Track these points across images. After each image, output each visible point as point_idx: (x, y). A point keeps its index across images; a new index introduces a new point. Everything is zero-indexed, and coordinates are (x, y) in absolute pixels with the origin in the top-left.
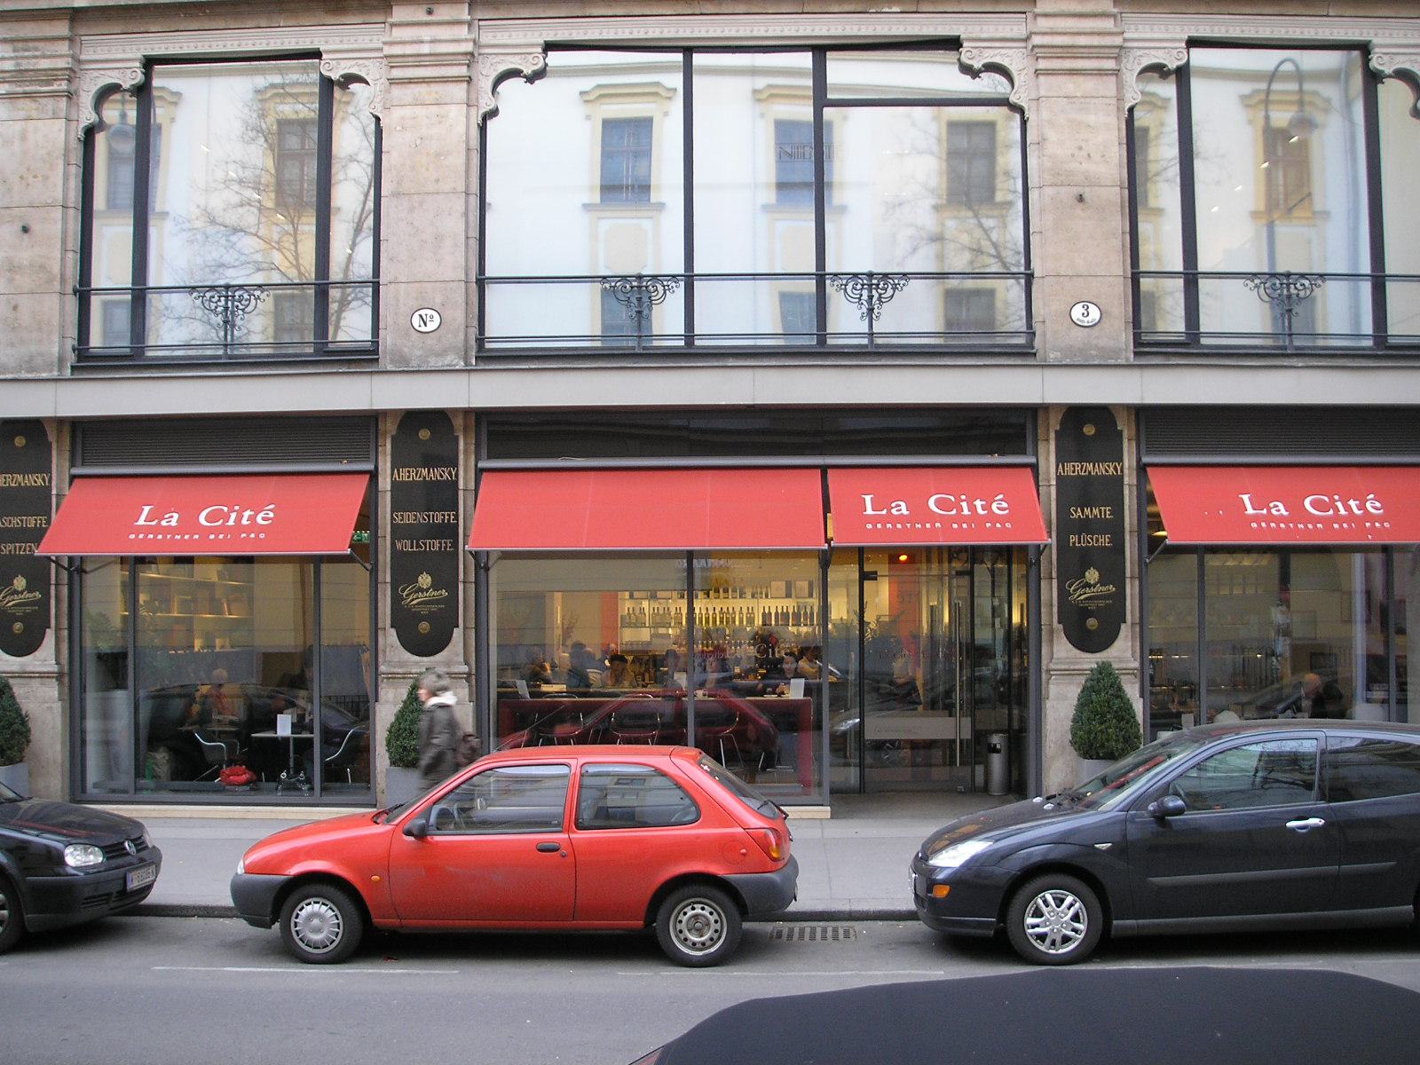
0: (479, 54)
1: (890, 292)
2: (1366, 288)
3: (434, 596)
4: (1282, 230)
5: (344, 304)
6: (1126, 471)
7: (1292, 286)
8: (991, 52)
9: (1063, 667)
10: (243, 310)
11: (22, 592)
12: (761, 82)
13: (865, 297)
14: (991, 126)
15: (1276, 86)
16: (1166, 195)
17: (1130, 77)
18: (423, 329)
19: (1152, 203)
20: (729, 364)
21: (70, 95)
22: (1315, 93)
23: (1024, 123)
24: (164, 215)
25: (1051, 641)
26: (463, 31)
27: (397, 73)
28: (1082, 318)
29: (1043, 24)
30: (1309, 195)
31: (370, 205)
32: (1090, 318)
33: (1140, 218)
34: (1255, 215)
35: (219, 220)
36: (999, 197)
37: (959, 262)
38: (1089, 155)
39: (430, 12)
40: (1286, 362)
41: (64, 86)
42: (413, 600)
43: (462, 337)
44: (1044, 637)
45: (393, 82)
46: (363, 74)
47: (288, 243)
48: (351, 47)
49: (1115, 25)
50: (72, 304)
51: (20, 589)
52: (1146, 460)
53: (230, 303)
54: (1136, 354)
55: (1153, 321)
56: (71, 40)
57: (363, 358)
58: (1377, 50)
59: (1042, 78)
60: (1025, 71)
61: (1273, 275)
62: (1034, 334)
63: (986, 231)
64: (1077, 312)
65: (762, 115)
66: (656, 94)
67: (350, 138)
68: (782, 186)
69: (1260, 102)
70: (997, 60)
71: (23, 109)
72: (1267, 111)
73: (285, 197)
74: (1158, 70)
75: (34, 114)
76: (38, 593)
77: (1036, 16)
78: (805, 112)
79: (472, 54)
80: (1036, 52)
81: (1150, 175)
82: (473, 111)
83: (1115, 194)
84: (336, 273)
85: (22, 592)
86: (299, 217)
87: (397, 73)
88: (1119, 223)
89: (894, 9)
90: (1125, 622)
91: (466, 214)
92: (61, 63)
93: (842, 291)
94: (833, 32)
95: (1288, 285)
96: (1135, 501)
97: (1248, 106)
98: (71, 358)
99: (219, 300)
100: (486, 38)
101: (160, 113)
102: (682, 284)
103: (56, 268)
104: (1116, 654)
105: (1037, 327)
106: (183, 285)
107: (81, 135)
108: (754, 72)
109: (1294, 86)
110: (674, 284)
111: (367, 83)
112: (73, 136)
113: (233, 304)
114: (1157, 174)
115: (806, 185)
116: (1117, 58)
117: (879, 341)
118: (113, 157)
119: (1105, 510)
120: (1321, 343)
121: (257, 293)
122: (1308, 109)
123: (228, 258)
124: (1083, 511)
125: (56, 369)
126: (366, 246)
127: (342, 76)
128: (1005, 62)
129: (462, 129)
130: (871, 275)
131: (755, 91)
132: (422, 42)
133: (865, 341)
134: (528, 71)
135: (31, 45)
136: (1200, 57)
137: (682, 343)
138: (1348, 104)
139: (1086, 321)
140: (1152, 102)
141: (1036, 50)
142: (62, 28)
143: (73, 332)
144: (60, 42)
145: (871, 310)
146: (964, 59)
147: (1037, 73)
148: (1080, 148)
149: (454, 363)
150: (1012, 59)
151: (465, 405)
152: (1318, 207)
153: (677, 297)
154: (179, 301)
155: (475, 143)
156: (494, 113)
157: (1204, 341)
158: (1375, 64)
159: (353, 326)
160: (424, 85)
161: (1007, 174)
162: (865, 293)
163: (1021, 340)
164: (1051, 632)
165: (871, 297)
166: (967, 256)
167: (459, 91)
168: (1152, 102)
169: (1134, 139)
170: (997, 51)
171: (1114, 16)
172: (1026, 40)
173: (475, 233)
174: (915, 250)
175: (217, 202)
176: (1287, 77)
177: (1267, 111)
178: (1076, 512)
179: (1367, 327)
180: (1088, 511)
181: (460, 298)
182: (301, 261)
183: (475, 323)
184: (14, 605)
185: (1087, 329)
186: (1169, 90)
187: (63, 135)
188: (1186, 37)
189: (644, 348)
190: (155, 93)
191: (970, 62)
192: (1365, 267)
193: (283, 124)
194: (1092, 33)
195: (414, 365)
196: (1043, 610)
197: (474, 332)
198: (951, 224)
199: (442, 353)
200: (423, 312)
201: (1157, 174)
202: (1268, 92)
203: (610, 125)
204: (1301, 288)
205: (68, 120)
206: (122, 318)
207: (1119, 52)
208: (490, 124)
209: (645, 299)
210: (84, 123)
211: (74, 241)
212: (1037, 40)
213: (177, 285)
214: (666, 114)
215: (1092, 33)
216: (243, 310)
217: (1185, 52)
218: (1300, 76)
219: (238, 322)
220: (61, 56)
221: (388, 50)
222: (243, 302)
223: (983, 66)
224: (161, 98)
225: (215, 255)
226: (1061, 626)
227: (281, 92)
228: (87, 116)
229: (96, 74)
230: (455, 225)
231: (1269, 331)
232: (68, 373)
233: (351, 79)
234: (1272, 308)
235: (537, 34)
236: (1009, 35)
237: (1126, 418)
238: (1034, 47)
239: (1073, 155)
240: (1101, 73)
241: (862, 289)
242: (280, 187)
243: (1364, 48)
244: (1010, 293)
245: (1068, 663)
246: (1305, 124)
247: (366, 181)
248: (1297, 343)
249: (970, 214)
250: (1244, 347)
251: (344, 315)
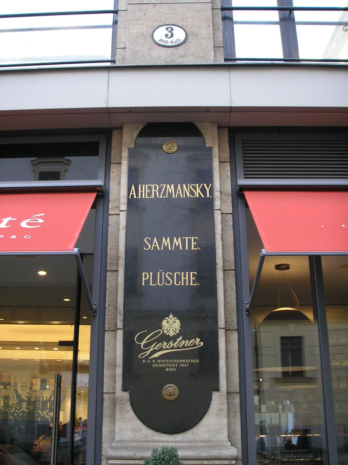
3: (184, 347)
6: (217, 194)
9: (125, 453)
11: (174, 338)
25: (113, 416)
28: (166, 39)
32: (174, 39)
42: (155, 351)
44: (106, 412)
51: (171, 334)
52: (242, 182)
76: (198, 340)
85: (174, 338)
90: (218, 390)
96: (231, 233)
104: (205, 436)
119: (190, 241)
124: (172, 241)
164: (114, 403)
178: (151, 242)
180: (166, 242)
184: (160, 357)
185: (171, 49)
196: (106, 372)
226: (126, 395)
237: (216, 135)
245: (134, 448)
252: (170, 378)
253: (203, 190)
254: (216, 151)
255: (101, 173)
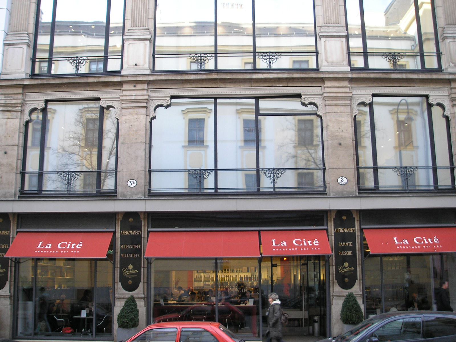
0: (150, 99)
1: (280, 174)
2: (431, 171)
4: (403, 152)
5: (106, 177)
6: (356, 231)
7: (408, 171)
8: (311, 99)
9: (337, 294)
10: (74, 179)
12: (239, 107)
13: (272, 176)
14: (312, 121)
15: (400, 107)
16: (367, 142)
17: (355, 106)
18: (131, 186)
19: (363, 144)
20: (229, 198)
21: (21, 111)
22: (412, 109)
23: (322, 121)
24: (50, 148)
26: (145, 92)
27: (124, 105)
29: (327, 90)
30: (412, 141)
31: (115, 146)
32: (344, 182)
33: (359, 149)
34: (395, 148)
35: (67, 150)
36: (315, 143)
37: (302, 164)
38: (342, 131)
39: (135, 86)
40: (406, 195)
41: (20, 108)
43: (143, 188)
45: (123, 108)
46: (113, 105)
47: (88, 157)
48: (109, 97)
49: (349, 90)
50: (19, 176)
51: (131, 269)
53: (69, 177)
54: (359, 193)
55: (364, 183)
56: (22, 94)
57: (112, 195)
58: (430, 97)
59: (327, 107)
60: (322, 105)
61: (402, 167)
62: (326, 187)
63: (311, 154)
64: (340, 180)
65: (239, 118)
66: (206, 111)
67: (109, 125)
68: (246, 141)
69: (395, 112)
70: (313, 101)
71: (6, 115)
72: (397, 115)
73: (88, 143)
74: (363, 104)
75: (10, 117)
77: (325, 87)
78: (253, 117)
79: (148, 99)
80: (325, 99)
81: (362, 136)
82: (148, 117)
83: (351, 143)
84: (103, 168)
85: (131, 270)
86: (92, 150)
87: (124, 105)
88: (352, 152)
89: (280, 86)
91: (145, 149)
92: (19, 101)
93: (265, 174)
94: (261, 93)
95: (406, 170)
96: (359, 240)
97: (392, 114)
98: (18, 194)
99: (66, 176)
100: (152, 94)
101: (49, 116)
102: (214, 172)
103: (15, 165)
105: (327, 185)
106: (55, 171)
107: (24, 123)
108: (236, 104)
109: (406, 107)
110: (211, 172)
111: (115, 108)
112: (22, 124)
113: (70, 177)
114: (364, 135)
115: (253, 141)
116: (350, 100)
117: (277, 190)
118: (34, 130)
120: (417, 188)
121: (78, 174)
122: (410, 114)
123: (69, 162)
125: (13, 197)
126: (113, 159)
127: (107, 106)
128: (316, 102)
129: (144, 122)
130: (274, 169)
131: (237, 110)
132: (132, 96)
133: (272, 190)
134: (165, 105)
135: (10, 95)
136: (376, 99)
137: (214, 191)
138: (423, 113)
139: (343, 183)
140: (362, 113)
141: (325, 98)
142: (20, 91)
143: (19, 185)
144: (19, 95)
145: (274, 180)
146: (303, 101)
147: (326, 105)
148: (340, 128)
149: (141, 197)
150: (318, 101)
151: (144, 210)
152: (415, 144)
153: (212, 176)
154: (54, 176)
155: (148, 127)
156: (154, 118)
157: (380, 189)
158: (430, 101)
159: (108, 184)
160: (133, 109)
161: (317, 136)
162: (272, 175)
163: (322, 189)
164: (333, 283)
165: (274, 176)
166: (304, 162)
167: (143, 111)
168: (362, 113)
169: (356, 124)
170: (312, 98)
171: (349, 87)
172: (322, 95)
173: (148, 156)
174: (288, 160)
175: (66, 144)
176: (403, 105)
177: (397, 115)
179: (432, 183)
180: (344, 244)
181: (143, 176)
182: (92, 163)
183: (148, 184)
184: (128, 274)
186: (367, 109)
187: (18, 124)
188: (371, 94)
189: (202, 193)
190: (48, 110)
191: (304, 102)
192: (430, 165)
193: (88, 120)
194: (342, 93)
195: (128, 198)
197: (147, 187)
198: (299, 152)
199: (137, 194)
200: (131, 181)
201: (364, 135)
202: (398, 109)
203: (191, 121)
204: (410, 171)
205: (21, 119)
206: (35, 180)
207: (351, 98)
208: (153, 121)
209: (202, 177)
210: (26, 120)
211: (21, 157)
212: (325, 95)
213: (53, 171)
214: (209, 117)
215: (342, 93)
216: (74, 179)
217: (371, 98)
218: (407, 104)
219: (80, 69)
220: (20, 99)
221: (121, 98)
222: (74, 177)
223: (309, 103)
224: (50, 111)
225: (65, 161)
226: (336, 281)
227: (87, 110)
228: (27, 118)
229: (30, 105)
230: (141, 153)
231: (401, 185)
232: (17, 198)
233: (109, 107)
234: (401, 178)
235: (168, 93)
236: (316, 93)
238: (324, 97)
239: (337, 131)
240: (345, 105)
241: (271, 174)
242: (86, 140)
243: (427, 97)
244: (319, 174)
246: (410, 119)
247: (113, 138)
248: (410, 189)
249: (305, 149)
250: (393, 190)
251: (106, 180)
252: (130, 279)
253: (353, 230)
254: (356, 219)
255: (114, 227)
